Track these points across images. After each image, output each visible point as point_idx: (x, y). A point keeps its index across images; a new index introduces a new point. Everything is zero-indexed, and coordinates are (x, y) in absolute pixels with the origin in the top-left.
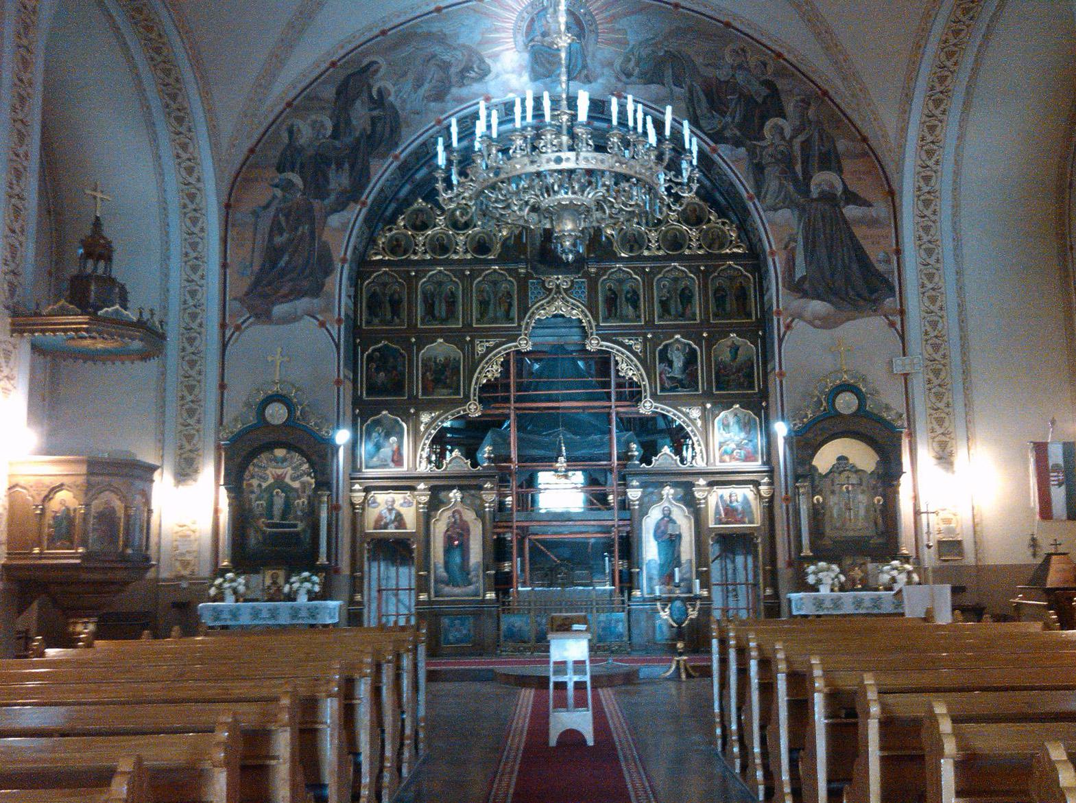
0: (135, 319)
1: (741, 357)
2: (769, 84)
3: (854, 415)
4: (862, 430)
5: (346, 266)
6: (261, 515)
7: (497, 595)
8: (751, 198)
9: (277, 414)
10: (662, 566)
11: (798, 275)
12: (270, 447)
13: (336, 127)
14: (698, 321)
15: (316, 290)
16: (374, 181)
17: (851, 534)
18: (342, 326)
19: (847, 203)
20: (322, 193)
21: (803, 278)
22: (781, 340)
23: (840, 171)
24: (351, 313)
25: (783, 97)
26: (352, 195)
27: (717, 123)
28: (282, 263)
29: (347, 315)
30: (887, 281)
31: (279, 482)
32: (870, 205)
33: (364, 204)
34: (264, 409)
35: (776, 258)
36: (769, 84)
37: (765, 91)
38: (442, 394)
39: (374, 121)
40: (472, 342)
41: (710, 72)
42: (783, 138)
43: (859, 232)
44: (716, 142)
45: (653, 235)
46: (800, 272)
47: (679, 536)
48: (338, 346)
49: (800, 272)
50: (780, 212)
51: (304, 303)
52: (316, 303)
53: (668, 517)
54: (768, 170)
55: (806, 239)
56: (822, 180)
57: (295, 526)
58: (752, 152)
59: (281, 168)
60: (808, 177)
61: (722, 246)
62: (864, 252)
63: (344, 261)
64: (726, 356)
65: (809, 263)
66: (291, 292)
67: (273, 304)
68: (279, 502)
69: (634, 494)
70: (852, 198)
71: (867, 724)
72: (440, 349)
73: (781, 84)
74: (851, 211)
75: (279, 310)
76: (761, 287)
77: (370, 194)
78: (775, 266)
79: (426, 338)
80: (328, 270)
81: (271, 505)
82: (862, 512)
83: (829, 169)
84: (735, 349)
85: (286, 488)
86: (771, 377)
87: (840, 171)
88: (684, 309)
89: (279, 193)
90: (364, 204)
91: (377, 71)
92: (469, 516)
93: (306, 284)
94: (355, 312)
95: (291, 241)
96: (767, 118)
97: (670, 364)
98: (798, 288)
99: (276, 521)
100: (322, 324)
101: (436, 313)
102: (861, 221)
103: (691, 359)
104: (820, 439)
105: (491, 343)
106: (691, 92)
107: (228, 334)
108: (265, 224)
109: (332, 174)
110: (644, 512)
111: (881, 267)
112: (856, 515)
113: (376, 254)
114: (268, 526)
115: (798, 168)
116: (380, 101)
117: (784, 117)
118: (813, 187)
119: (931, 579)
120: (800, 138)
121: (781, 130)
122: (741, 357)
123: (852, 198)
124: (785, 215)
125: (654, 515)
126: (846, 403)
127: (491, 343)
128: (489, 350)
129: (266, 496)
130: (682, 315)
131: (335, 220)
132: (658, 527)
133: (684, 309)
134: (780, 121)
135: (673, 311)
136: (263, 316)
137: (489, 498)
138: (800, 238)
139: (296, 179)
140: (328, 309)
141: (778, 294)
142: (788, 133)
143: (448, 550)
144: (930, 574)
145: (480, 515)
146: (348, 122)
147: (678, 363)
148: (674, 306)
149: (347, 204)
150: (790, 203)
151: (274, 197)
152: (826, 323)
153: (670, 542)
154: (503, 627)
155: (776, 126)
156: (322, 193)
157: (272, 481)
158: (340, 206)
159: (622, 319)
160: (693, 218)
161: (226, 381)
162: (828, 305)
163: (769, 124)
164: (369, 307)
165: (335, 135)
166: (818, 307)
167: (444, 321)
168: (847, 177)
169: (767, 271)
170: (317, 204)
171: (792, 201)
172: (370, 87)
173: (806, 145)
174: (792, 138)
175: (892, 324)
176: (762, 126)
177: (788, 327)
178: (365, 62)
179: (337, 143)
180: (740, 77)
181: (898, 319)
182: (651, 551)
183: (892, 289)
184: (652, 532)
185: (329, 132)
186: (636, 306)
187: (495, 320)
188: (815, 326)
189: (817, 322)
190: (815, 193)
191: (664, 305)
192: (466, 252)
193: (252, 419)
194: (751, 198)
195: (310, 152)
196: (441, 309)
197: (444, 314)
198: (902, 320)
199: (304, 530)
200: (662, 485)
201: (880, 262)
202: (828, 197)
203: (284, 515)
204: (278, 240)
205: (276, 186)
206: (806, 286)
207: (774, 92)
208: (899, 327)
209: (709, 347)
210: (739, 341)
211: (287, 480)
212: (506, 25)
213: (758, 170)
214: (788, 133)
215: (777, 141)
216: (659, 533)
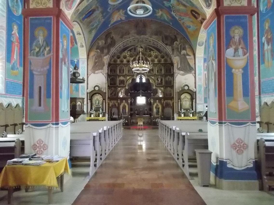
0: (82, 78)
1: (170, 80)
2: (175, 36)
3: (187, 89)
6: (95, 104)
8: (172, 54)
9: (97, 88)
11: (179, 67)
12: (96, 93)
15: (102, 69)
17: (186, 108)
19: (187, 56)
23: (186, 51)
24: (107, 72)
26: (108, 53)
27: (166, 42)
28: (97, 64)
30: (193, 68)
32: (190, 56)
33: (110, 55)
34: (95, 88)
35: (175, 64)
36: (175, 36)
37: (174, 37)
38: (122, 85)
39: (111, 42)
40: (127, 77)
41: (166, 34)
44: (166, 45)
46: (179, 67)
47: (159, 108)
49: (179, 67)
50: (176, 57)
53: (157, 105)
54: (175, 50)
57: (100, 106)
58: (172, 47)
60: (181, 51)
61: (167, 62)
68: (97, 102)
69: (152, 101)
71: (232, 169)
72: (122, 78)
73: (177, 36)
74: (188, 57)
75: (96, 72)
76: (173, 68)
78: (175, 66)
79: (119, 76)
80: (104, 66)
81: (96, 102)
82: (188, 105)
83: (184, 50)
84: (169, 79)
87: (186, 51)
89: (96, 53)
90: (110, 55)
91: (112, 33)
92: (126, 104)
94: (108, 72)
95: (98, 61)
96: (174, 42)
97: (158, 81)
98: (179, 69)
99: (97, 105)
100: (103, 74)
101: (121, 72)
102: (189, 59)
103: (162, 80)
105: (130, 77)
106: (162, 37)
107: (88, 76)
108: (94, 58)
109: (104, 50)
110: (154, 104)
111: (192, 66)
112: (187, 105)
113: (111, 62)
114: (96, 106)
115: (179, 50)
116: (112, 38)
117: (177, 41)
118: (182, 53)
119: (110, 120)
122: (170, 80)
124: (177, 57)
125: (155, 105)
126: (186, 88)
127: (130, 77)
128: (130, 78)
130: (160, 73)
131: (105, 57)
135: (159, 72)
136: (94, 73)
137: (129, 101)
138: (179, 62)
139: (99, 51)
141: (176, 70)
142: (178, 44)
145: (128, 104)
147: (160, 80)
148: (159, 71)
149: (107, 55)
150: (178, 56)
152: (183, 75)
153: (157, 108)
154: (131, 121)
157: (96, 99)
158: (106, 55)
159: (151, 73)
161: (88, 83)
162: (184, 72)
163: (175, 43)
164: (110, 71)
165: (105, 43)
166: (182, 72)
167: (122, 73)
168: (187, 51)
169: (174, 66)
173: (181, 46)
175: (193, 75)
176: (174, 43)
177: (177, 75)
179: (105, 45)
180: (171, 34)
181: (194, 74)
182: (155, 110)
183: (193, 70)
185: (104, 43)
186: (153, 71)
189: (182, 75)
190: (182, 53)
191: (157, 71)
192: (126, 62)
194: (172, 54)
195: (101, 46)
197: (122, 72)
198: (195, 75)
201: (192, 65)
202: (184, 55)
203: (98, 104)
204: (96, 61)
205: (96, 52)
206: (180, 69)
208: (194, 76)
210: (169, 77)
211: (99, 99)
212: (141, 50)
213: (173, 50)
214: (178, 44)
215: (176, 45)
216: (156, 108)
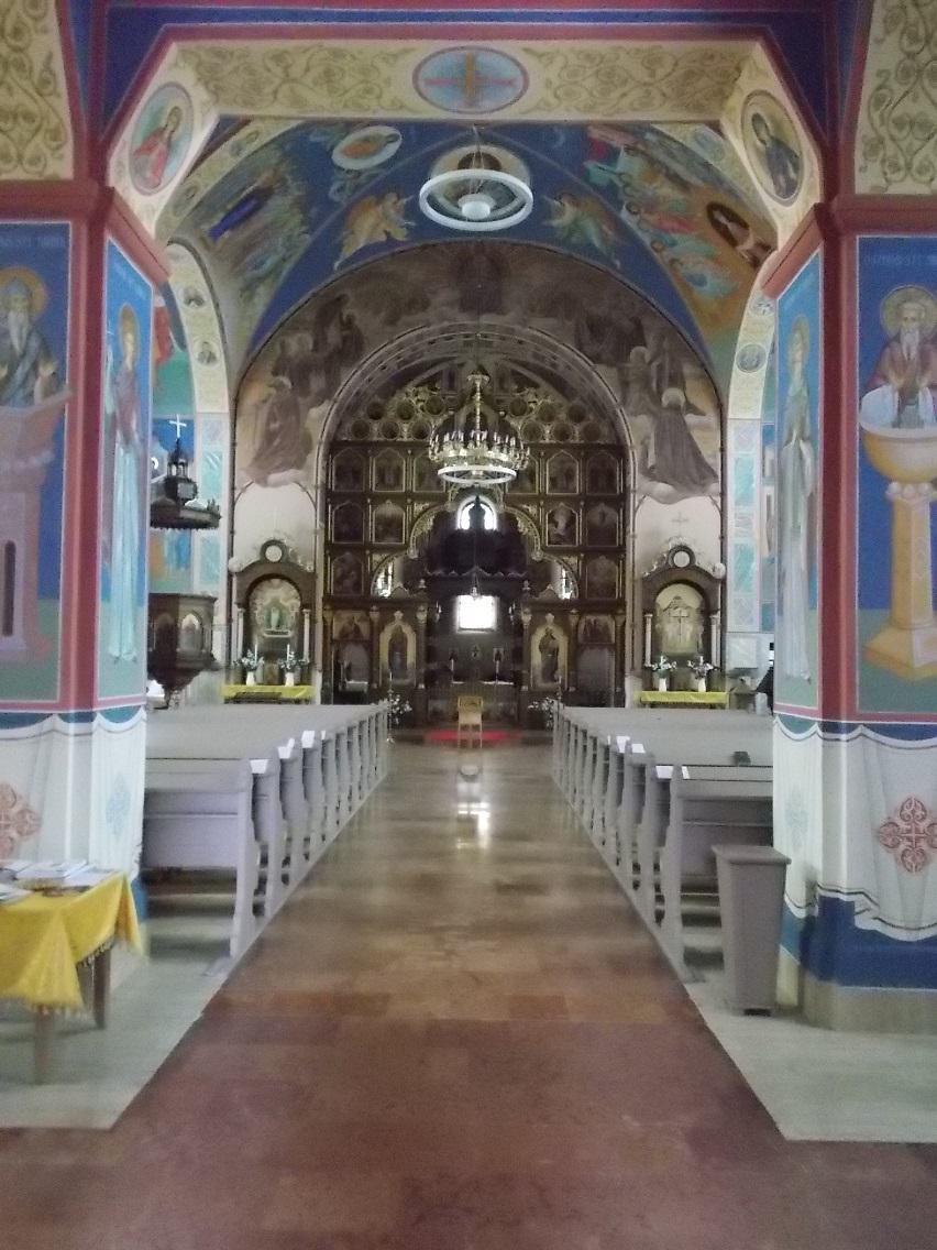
3: (686, 568)
4: (689, 578)
5: (322, 448)
7: (426, 686)
9: (274, 554)
10: (544, 669)
11: (650, 464)
12: (269, 577)
13: (316, 343)
14: (537, 493)
16: (343, 383)
18: (319, 492)
20: (305, 391)
21: (653, 467)
22: (635, 512)
25: (645, 332)
26: (325, 395)
28: (276, 443)
29: (322, 482)
31: (276, 603)
38: (390, 541)
39: (345, 340)
42: (644, 362)
43: (696, 435)
44: (594, 362)
45: (420, 415)
46: (651, 462)
48: (315, 506)
49: (651, 462)
51: (291, 473)
52: (300, 473)
53: (549, 636)
55: (657, 435)
56: (671, 395)
57: (285, 633)
59: (276, 373)
60: (660, 393)
62: (697, 449)
63: (320, 443)
64: (596, 519)
65: (658, 454)
66: (282, 465)
67: (269, 473)
68: (275, 617)
70: (691, 408)
72: (389, 509)
74: (690, 419)
75: (273, 477)
76: (624, 471)
77: (341, 394)
78: (634, 457)
79: (379, 500)
80: (308, 450)
81: (269, 620)
82: (688, 636)
84: (603, 515)
85: (281, 608)
86: (627, 537)
88: (567, 484)
89: (273, 391)
92: (407, 630)
93: (293, 459)
98: (650, 473)
99: (273, 629)
100: (304, 489)
103: (571, 521)
104: (658, 586)
110: (532, 632)
111: (709, 461)
115: (654, 385)
116: (348, 324)
118: (663, 399)
120: (655, 364)
121: (642, 357)
123: (691, 408)
125: (540, 634)
126: (682, 560)
128: (425, 510)
129: (266, 611)
130: (566, 489)
131: (314, 412)
132: (542, 641)
133: (567, 484)
134: (642, 349)
135: (559, 486)
136: (263, 482)
137: (422, 617)
139: (286, 381)
140: (308, 478)
141: (636, 480)
143: (391, 654)
144: (613, 700)
145: (416, 630)
146: (325, 339)
147: (562, 523)
148: (562, 482)
151: (270, 395)
152: (668, 500)
154: (430, 709)
155: (637, 353)
156: (305, 391)
160: (546, 417)
161: (719, 542)
166: (662, 488)
167: (391, 487)
170: (300, 400)
171: (648, 410)
172: (341, 315)
173: (661, 368)
174: (651, 362)
175: (714, 503)
177: (641, 502)
178: (337, 295)
181: (719, 499)
182: (537, 659)
183: (716, 476)
184: (537, 647)
185: (311, 346)
187: (429, 488)
188: (659, 501)
190: (665, 401)
193: (255, 558)
196: (390, 479)
197: (392, 482)
199: (293, 637)
200: (546, 612)
202: (675, 408)
206: (655, 472)
207: (639, 327)
209: (585, 512)
213: (625, 385)
214: (648, 358)
